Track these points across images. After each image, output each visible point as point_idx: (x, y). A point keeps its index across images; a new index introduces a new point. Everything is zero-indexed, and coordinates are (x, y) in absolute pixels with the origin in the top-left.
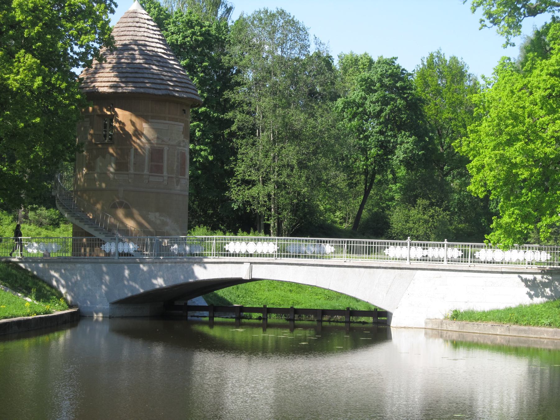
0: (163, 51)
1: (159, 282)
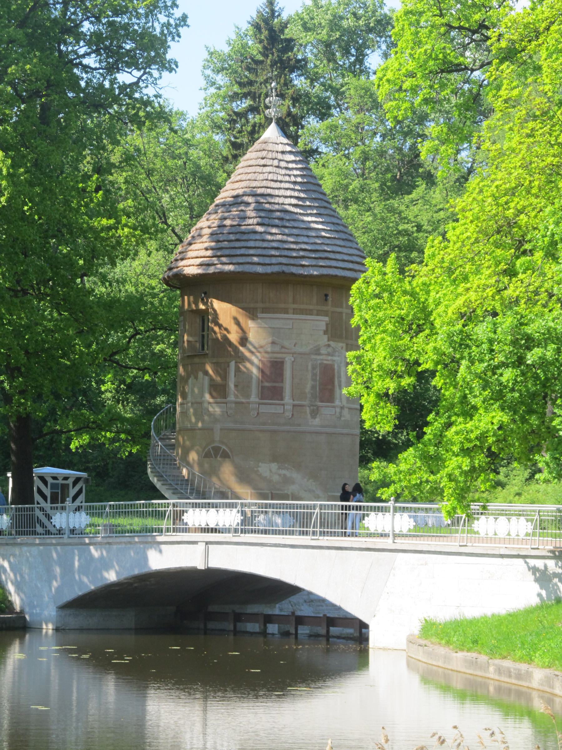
0: (294, 201)
1: (112, 576)
